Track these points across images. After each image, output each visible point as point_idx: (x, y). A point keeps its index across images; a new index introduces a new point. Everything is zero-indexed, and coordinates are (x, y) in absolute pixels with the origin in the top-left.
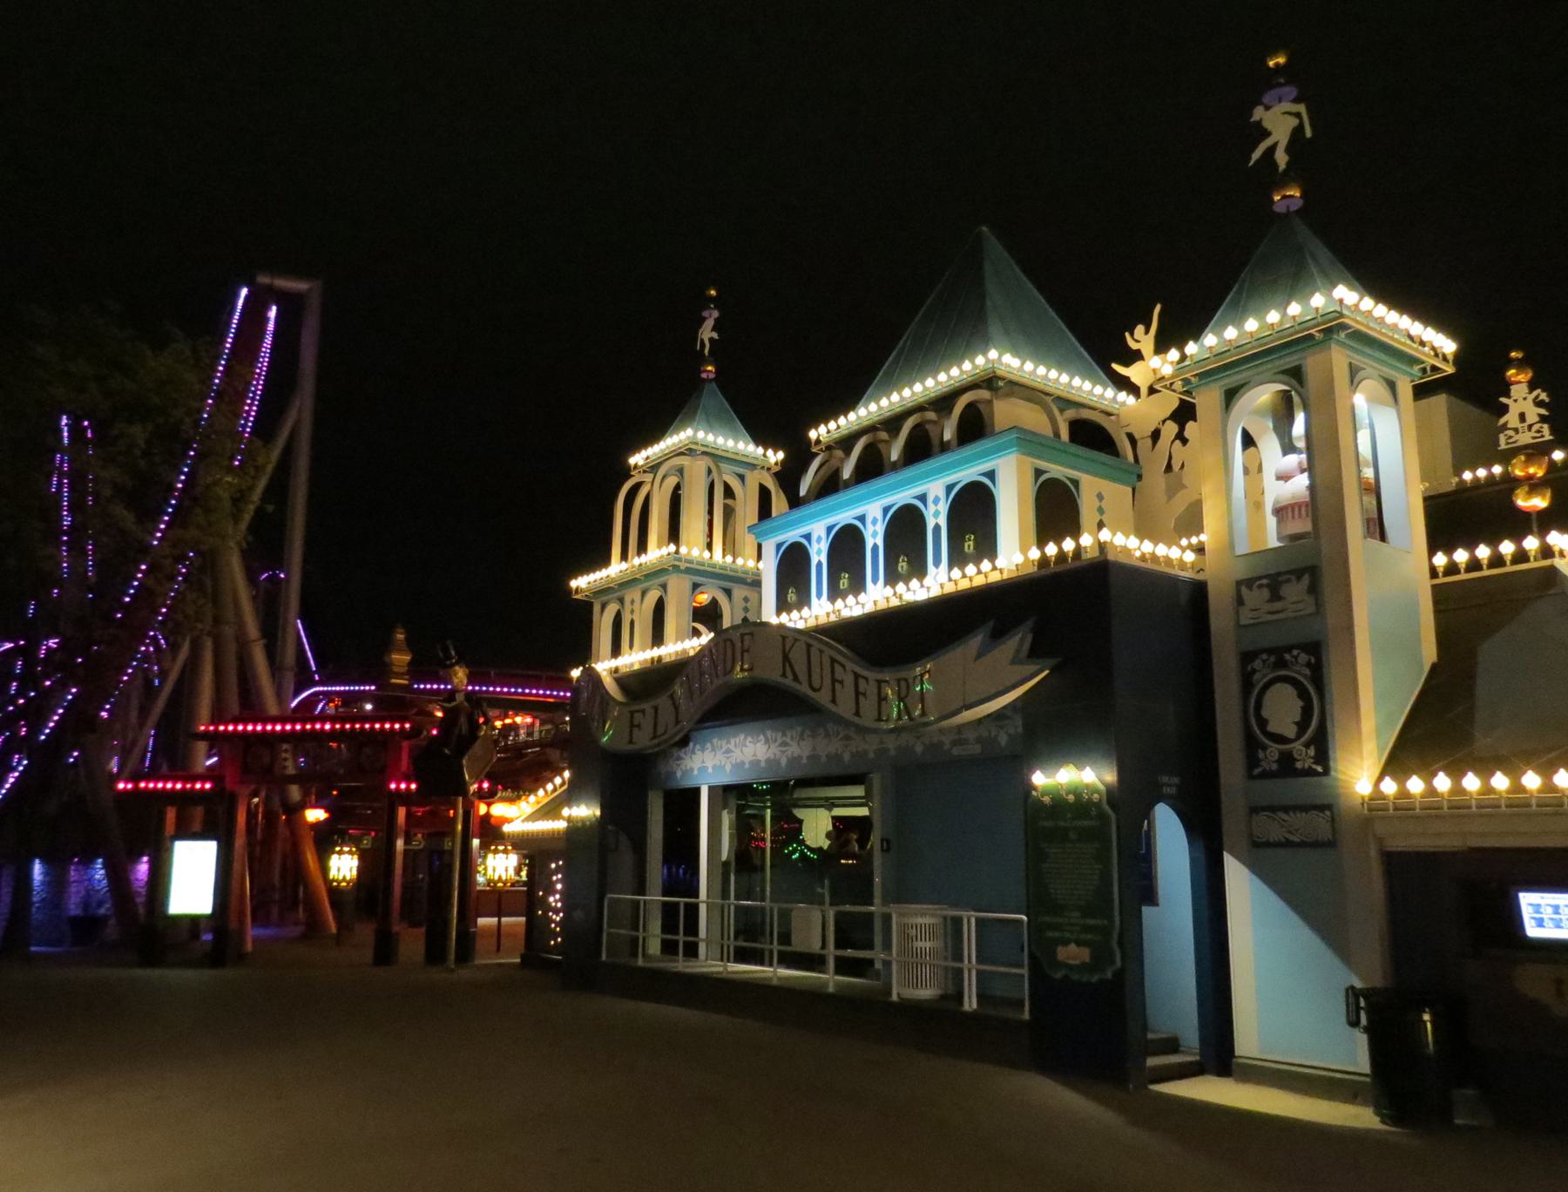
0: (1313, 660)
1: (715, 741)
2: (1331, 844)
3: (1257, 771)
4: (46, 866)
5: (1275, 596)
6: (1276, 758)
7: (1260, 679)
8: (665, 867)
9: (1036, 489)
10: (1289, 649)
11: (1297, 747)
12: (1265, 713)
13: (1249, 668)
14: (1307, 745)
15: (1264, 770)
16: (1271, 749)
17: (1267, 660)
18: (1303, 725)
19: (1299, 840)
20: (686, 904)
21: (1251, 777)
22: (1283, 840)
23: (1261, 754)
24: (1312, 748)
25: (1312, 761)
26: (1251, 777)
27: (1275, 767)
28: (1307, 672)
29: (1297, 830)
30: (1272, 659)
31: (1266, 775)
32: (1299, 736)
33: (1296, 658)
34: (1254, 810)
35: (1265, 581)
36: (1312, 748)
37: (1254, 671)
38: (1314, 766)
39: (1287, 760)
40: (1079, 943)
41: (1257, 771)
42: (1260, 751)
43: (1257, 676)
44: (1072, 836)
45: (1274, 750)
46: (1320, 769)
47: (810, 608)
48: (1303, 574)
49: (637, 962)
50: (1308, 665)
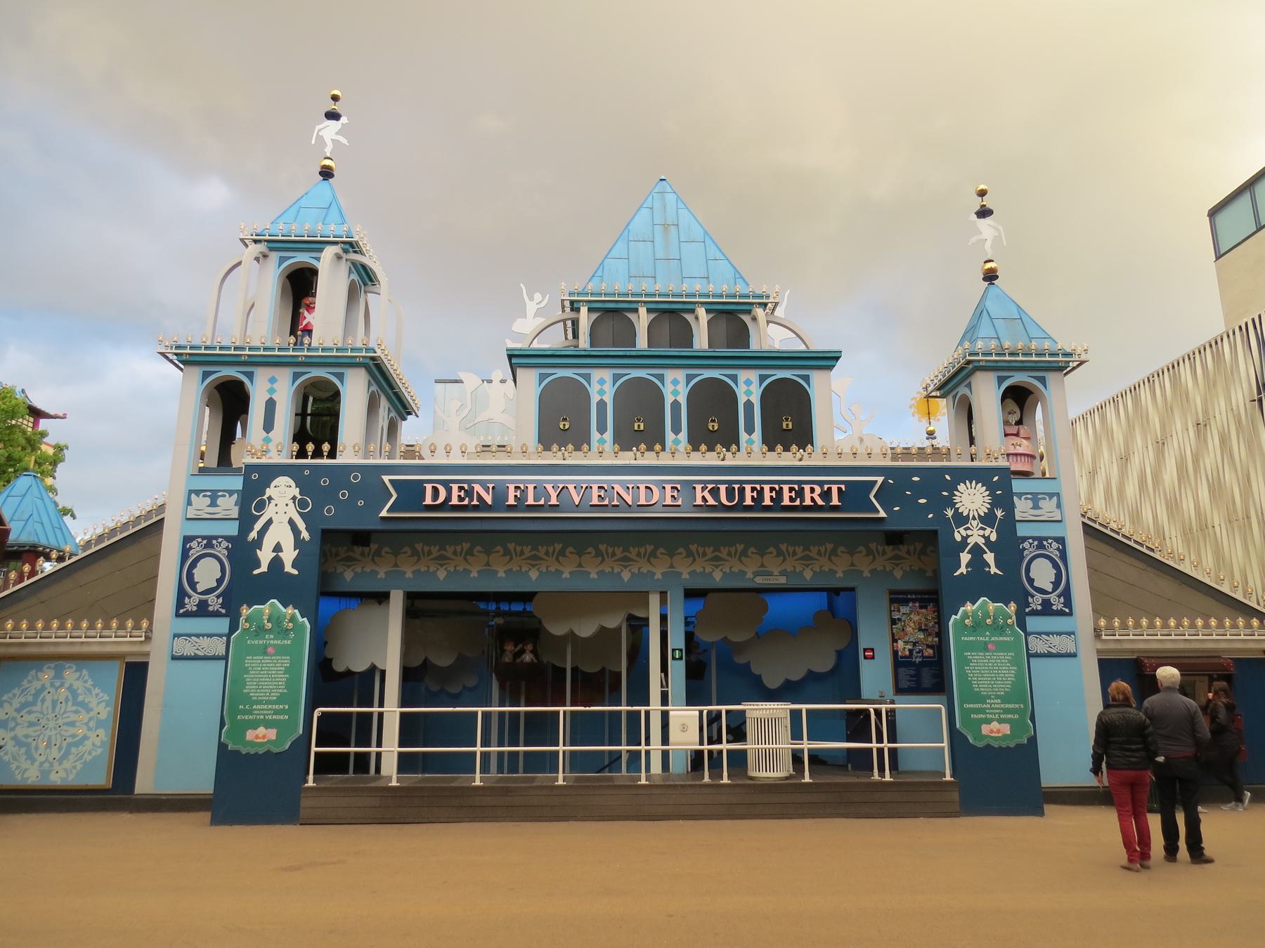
0: (230, 546)
2: (1074, 655)
3: (181, 611)
5: (1036, 507)
6: (1040, 602)
7: (194, 554)
9: (369, 395)
10: (216, 538)
11: (1053, 598)
12: (1032, 575)
13: (188, 546)
14: (1059, 597)
15: (188, 610)
18: (1056, 584)
19: (1055, 652)
21: (178, 615)
22: (193, 654)
23: (1030, 600)
24: (1062, 598)
26: (178, 615)
27: (1039, 608)
28: (226, 552)
29: (1054, 646)
30: (1036, 543)
31: (188, 614)
32: (1054, 590)
33: (1051, 544)
34: (176, 636)
35: (209, 493)
36: (1062, 598)
37: (191, 548)
38: (220, 610)
39: (1047, 604)
40: (1000, 721)
41: (181, 611)
43: (1026, 552)
45: (196, 598)
46: (1067, 610)
47: (812, 445)
48: (1053, 496)
49: (556, 779)
50: (1058, 549)
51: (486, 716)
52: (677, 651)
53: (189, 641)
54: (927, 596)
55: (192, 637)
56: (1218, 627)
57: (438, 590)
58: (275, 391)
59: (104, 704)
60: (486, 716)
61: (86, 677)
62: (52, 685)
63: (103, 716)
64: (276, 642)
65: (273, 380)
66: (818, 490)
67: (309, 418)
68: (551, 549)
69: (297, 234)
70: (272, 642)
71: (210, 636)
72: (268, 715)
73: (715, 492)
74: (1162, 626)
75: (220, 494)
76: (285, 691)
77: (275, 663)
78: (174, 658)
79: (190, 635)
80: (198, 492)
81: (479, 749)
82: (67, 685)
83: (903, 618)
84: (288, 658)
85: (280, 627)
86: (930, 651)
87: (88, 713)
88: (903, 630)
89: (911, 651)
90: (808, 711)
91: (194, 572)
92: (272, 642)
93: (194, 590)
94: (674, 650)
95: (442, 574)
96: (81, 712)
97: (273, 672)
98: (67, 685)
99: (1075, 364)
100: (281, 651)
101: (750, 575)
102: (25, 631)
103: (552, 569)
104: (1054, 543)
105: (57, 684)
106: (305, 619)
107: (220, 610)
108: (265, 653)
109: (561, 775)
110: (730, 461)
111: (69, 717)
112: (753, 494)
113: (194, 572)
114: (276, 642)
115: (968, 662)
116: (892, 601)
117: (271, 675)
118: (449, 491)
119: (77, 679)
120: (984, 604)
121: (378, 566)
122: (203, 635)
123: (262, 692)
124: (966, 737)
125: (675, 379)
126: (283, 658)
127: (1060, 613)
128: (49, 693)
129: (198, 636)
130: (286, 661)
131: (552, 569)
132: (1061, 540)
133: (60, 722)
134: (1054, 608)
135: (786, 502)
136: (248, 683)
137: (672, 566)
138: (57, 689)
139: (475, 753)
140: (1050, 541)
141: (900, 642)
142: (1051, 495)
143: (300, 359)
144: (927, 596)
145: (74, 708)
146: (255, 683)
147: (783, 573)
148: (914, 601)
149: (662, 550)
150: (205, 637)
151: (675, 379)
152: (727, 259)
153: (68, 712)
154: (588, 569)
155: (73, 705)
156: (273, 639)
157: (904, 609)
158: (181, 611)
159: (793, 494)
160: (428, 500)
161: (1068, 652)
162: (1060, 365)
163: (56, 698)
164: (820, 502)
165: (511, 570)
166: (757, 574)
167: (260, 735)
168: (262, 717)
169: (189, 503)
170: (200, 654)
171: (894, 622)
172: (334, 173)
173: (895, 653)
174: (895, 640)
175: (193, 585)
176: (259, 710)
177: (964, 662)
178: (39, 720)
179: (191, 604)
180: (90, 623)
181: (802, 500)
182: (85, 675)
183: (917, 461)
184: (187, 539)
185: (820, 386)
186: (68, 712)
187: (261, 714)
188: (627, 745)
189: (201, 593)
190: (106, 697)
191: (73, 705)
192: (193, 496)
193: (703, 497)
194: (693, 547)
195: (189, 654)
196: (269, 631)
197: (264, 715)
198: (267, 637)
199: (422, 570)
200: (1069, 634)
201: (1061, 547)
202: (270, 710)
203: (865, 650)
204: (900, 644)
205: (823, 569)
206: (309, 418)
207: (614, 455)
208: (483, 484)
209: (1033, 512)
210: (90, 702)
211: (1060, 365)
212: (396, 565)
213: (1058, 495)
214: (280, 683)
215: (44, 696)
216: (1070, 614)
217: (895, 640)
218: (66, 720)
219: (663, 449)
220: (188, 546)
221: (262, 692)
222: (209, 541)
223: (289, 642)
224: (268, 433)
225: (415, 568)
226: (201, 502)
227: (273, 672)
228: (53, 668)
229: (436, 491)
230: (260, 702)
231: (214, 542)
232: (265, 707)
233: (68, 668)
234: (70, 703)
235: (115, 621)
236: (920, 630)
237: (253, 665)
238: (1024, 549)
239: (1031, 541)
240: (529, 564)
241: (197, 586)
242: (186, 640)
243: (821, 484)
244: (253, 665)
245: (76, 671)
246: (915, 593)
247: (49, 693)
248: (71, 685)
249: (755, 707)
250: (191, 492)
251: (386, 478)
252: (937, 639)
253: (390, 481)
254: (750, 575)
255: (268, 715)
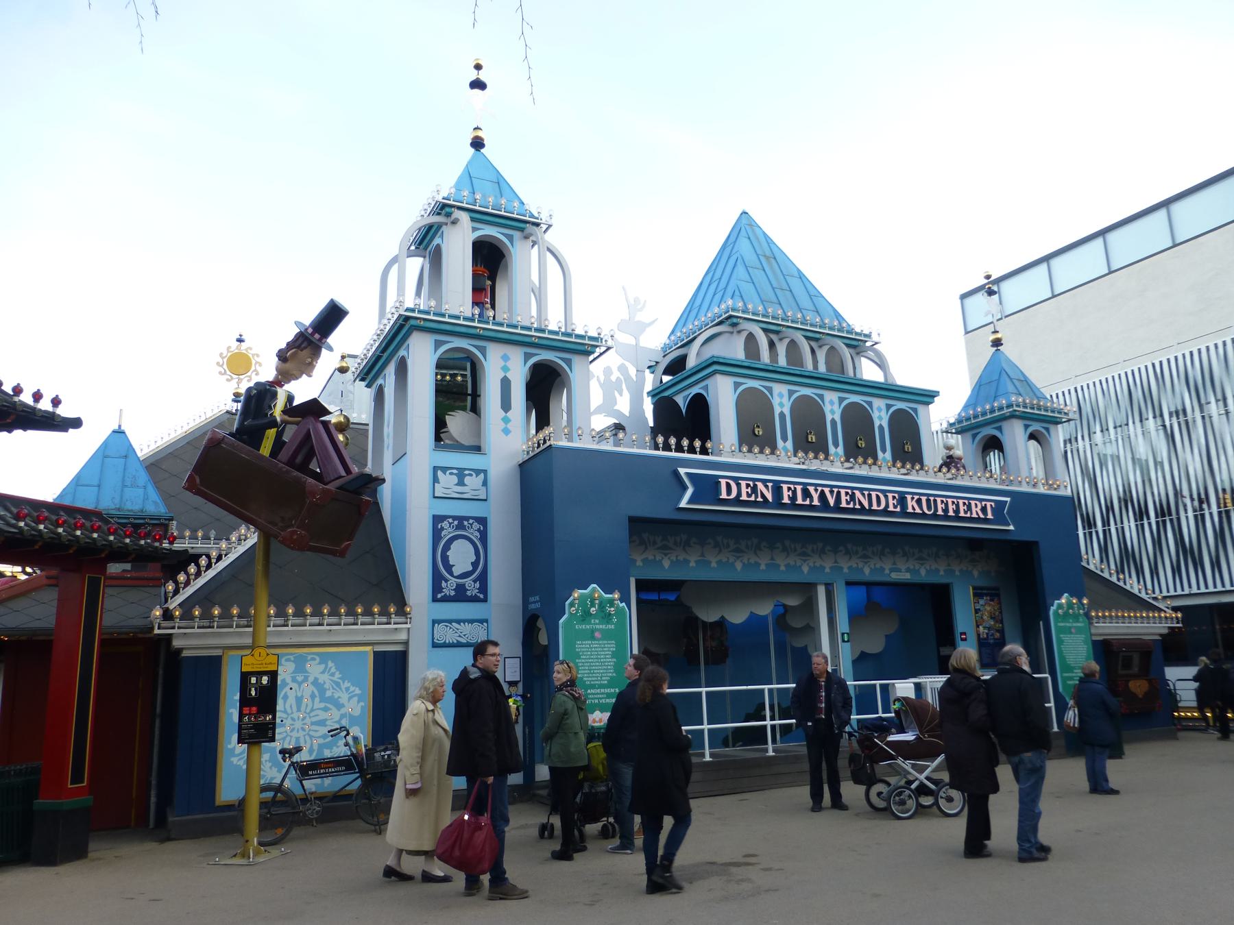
1: (719, 539)
3: (439, 596)
4: (605, 726)
5: (461, 483)
8: (1158, 638)
10: (467, 518)
11: (468, 582)
14: (475, 581)
16: (451, 581)
17: (452, 523)
20: (881, 685)
21: (435, 600)
22: (455, 642)
23: (444, 584)
25: (478, 591)
26: (435, 600)
28: (478, 534)
30: (456, 522)
31: (446, 599)
33: (471, 525)
35: (455, 471)
37: (442, 529)
38: (478, 594)
41: (439, 596)
42: (443, 582)
44: (597, 634)
45: (453, 582)
49: (766, 750)
50: (479, 530)
51: (770, 691)
52: (846, 635)
53: (450, 628)
54: (993, 592)
55: (453, 624)
56: (381, 614)
57: (652, 578)
58: (509, 370)
59: (356, 699)
60: (770, 691)
61: (333, 670)
62: (294, 680)
63: (357, 712)
64: (601, 626)
65: (505, 358)
66: (979, 507)
67: (470, 391)
68: (678, 539)
69: (457, 198)
70: (597, 627)
71: (471, 621)
72: (601, 699)
73: (919, 502)
74: (275, 614)
75: (467, 472)
76: (614, 675)
77: (603, 648)
78: (435, 645)
79: (450, 621)
80: (444, 469)
81: (706, 727)
82: (311, 679)
83: (981, 609)
84: (613, 642)
85: (603, 611)
86: (998, 634)
87: (339, 710)
88: (982, 618)
89: (987, 634)
90: (707, 693)
91: (448, 554)
92: (597, 627)
93: (451, 574)
94: (843, 634)
95: (666, 563)
96: (331, 709)
97: (602, 656)
98: (311, 679)
99: (603, 349)
100: (607, 635)
101: (887, 571)
102: (236, 619)
103: (681, 558)
104: (476, 524)
105: (300, 679)
106: (624, 604)
107: (478, 594)
108: (593, 638)
109: (770, 746)
110: (913, 477)
111: (317, 715)
112: (747, 490)
113: (448, 554)
114: (601, 626)
115: (1063, 641)
116: (975, 595)
117: (600, 659)
118: (738, 485)
119: (323, 672)
120: (594, 590)
121: (759, 557)
122: (464, 621)
123: (594, 677)
124: (1065, 698)
125: (780, 393)
126: (609, 642)
127: (474, 599)
128: (291, 689)
129: (458, 622)
130: (611, 646)
131: (681, 558)
132: (483, 521)
133: (308, 721)
134: (469, 593)
135: (844, 505)
136: (580, 668)
137: (836, 562)
138: (300, 684)
139: (702, 731)
140: (471, 521)
141: (980, 627)
142: (478, 472)
143: (533, 339)
144: (993, 592)
145: (322, 705)
146: (587, 668)
147: (908, 570)
148: (986, 595)
149: (764, 544)
150: (466, 624)
151: (780, 393)
152: (753, 283)
153: (316, 710)
154: (842, 565)
155: (320, 702)
156: (599, 624)
157: (982, 602)
158: (437, 594)
159: (749, 490)
160: (724, 496)
161: (447, 642)
162: (585, 348)
163: (299, 694)
164: (982, 516)
165: (720, 561)
166: (892, 570)
167: (597, 719)
168: (596, 701)
169: (436, 480)
170: (463, 641)
171: (977, 611)
172: (485, 143)
173: (979, 635)
174: (978, 626)
175: (449, 568)
176: (594, 694)
177: (1060, 642)
178: (282, 721)
179: (449, 587)
180: (331, 609)
181: (971, 514)
182: (331, 668)
183: (637, 448)
184: (437, 519)
185: (577, 371)
186: (316, 710)
187: (596, 698)
188: (857, 715)
189: (458, 577)
190: (358, 691)
191: (320, 702)
192: (440, 473)
193: (913, 506)
194: (645, 536)
195: (451, 642)
196: (595, 616)
197: (598, 699)
198: (592, 621)
199: (724, 561)
200: (481, 621)
201: (482, 529)
202: (602, 694)
203: (962, 634)
204: (981, 628)
205: (816, 564)
206: (470, 391)
207: (887, 469)
208: (764, 482)
209: (460, 489)
210: (339, 697)
211: (585, 348)
212: (703, 555)
213: (485, 472)
214: (609, 667)
215: (286, 693)
216: (485, 600)
217: (978, 626)
218: (314, 719)
219: (922, 468)
220: (439, 527)
221: (594, 677)
222: (461, 521)
223: (613, 627)
224: (506, 412)
225: (644, 556)
226: (448, 482)
227: (602, 656)
228: (293, 661)
229: (728, 486)
230: (593, 687)
231: (466, 523)
232: (598, 691)
233: (310, 660)
234: (317, 700)
235: (197, 608)
236: (991, 618)
237: (583, 650)
238: (442, 529)
239: (451, 520)
240: (734, 556)
241: (453, 569)
242: (447, 626)
243: (981, 500)
244: (583, 650)
245: (320, 663)
246: (988, 589)
247: (291, 689)
248: (316, 679)
249: (934, 680)
250: (435, 469)
251: (682, 471)
252: (1001, 625)
253: (687, 474)
254: (887, 571)
255: (601, 699)
